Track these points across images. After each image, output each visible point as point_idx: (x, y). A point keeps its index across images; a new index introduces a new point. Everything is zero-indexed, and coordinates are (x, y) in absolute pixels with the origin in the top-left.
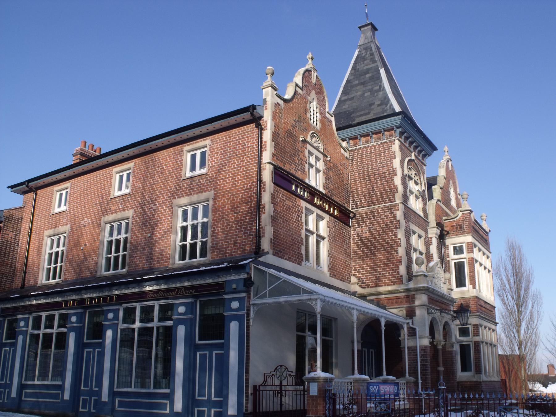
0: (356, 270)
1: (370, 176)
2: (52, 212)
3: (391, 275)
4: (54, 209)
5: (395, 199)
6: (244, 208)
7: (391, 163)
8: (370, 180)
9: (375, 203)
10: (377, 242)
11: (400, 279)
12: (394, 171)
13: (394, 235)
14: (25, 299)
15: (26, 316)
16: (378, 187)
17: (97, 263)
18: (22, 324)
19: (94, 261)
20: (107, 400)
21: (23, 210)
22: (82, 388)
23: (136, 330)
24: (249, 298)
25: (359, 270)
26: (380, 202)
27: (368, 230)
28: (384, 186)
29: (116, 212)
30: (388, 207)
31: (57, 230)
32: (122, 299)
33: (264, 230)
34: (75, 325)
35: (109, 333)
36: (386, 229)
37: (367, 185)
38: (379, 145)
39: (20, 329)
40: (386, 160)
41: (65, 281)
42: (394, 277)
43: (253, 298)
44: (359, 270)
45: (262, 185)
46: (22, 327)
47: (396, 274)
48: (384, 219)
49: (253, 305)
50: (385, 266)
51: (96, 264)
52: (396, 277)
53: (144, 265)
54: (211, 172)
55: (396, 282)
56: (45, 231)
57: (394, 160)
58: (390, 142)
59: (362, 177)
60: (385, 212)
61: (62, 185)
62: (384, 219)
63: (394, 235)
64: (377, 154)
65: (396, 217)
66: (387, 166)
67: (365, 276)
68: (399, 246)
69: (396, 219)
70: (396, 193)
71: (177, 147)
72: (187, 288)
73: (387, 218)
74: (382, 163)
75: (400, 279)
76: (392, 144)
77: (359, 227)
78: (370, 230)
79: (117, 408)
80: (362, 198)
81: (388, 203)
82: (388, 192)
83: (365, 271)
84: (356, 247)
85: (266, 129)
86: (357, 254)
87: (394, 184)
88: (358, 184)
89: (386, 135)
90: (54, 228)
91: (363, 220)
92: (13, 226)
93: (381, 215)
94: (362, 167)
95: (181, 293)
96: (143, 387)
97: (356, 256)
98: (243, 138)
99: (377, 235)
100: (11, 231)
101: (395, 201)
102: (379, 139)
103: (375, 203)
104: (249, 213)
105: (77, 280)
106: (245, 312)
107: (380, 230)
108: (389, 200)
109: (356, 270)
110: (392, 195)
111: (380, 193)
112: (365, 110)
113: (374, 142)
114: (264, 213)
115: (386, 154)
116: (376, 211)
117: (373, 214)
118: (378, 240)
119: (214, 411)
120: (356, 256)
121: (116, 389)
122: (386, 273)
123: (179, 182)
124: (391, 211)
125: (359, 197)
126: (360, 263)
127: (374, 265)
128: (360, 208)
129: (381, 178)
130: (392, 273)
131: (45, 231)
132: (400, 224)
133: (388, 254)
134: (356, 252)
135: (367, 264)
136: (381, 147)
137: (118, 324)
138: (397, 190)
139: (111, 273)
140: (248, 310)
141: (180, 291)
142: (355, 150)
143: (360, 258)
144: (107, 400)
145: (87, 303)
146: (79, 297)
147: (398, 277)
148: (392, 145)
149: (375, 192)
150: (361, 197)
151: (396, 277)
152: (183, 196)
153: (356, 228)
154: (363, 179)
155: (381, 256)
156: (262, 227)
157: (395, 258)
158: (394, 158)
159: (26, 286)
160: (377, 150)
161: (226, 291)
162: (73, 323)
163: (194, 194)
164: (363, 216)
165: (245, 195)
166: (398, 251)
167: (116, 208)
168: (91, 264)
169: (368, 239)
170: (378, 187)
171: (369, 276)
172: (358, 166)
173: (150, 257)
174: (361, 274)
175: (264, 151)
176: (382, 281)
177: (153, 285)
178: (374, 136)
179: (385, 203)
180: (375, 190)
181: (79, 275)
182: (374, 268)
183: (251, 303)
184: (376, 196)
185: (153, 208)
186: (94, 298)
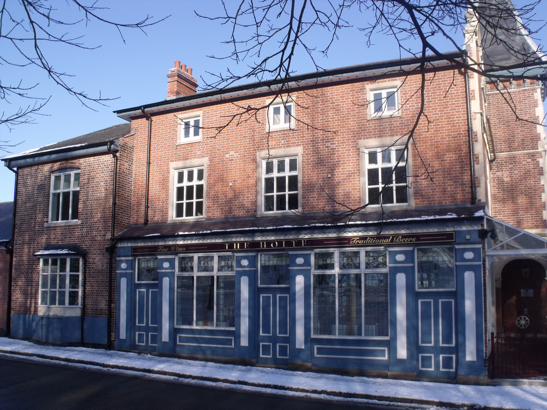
0: (497, 212)
1: (510, 122)
2: (178, 143)
3: (534, 219)
4: (180, 140)
5: (537, 147)
6: (450, 157)
7: (533, 111)
8: (510, 126)
9: (516, 148)
10: (519, 187)
11: (544, 223)
12: (537, 119)
13: (537, 181)
14: (166, 239)
15: (173, 257)
16: (519, 133)
17: (256, 201)
18: (166, 265)
19: (251, 199)
20: (303, 347)
21: (134, 138)
22: (261, 334)
23: (337, 275)
24: (484, 249)
25: (500, 212)
26: (522, 148)
27: (509, 175)
28: (525, 133)
29: (277, 148)
30: (531, 154)
31: (188, 163)
32: (312, 244)
33: (479, 180)
34: (247, 269)
35: (300, 280)
36: (527, 175)
37: (507, 130)
38: (519, 92)
39: (163, 271)
40: (527, 107)
41: (209, 219)
42: (537, 221)
43: (488, 249)
44: (500, 212)
45: (473, 134)
46: (166, 269)
47: (540, 219)
48: (526, 165)
49: (488, 255)
50: (527, 210)
51: (255, 203)
52: (539, 221)
53: (325, 207)
54: (406, 115)
55: (539, 225)
56: (170, 163)
57: (536, 109)
58: (531, 90)
59: (501, 123)
60: (527, 158)
61: (189, 112)
62: (526, 165)
63: (537, 181)
64: (517, 100)
65: (539, 164)
66: (529, 114)
67: (507, 218)
68: (542, 192)
69: (539, 166)
70: (539, 140)
71: (356, 84)
72: (404, 236)
73: (529, 165)
74: (523, 110)
75: (544, 223)
76: (533, 92)
77: (500, 171)
78: (511, 175)
79: (316, 355)
80: (502, 143)
81: (530, 150)
82: (530, 139)
83: (507, 214)
84: (496, 190)
85: (473, 78)
86: (497, 197)
87: (536, 132)
88: (497, 129)
89: (528, 82)
90: (183, 160)
91: (504, 164)
92: (127, 155)
93: (523, 161)
94: (501, 112)
95: (397, 240)
96: (350, 333)
97: (497, 199)
98: (444, 84)
99: (519, 180)
100: (126, 162)
101: (538, 149)
102: (518, 85)
103: (516, 148)
104: (459, 162)
105: (226, 218)
106: (481, 263)
107: (522, 176)
108: (531, 147)
109: (497, 212)
110: (534, 143)
111: (521, 140)
112: (503, 54)
113: (514, 88)
114: (478, 164)
115: (528, 101)
116: (517, 157)
117: (513, 160)
118: (519, 185)
119: (443, 357)
120: (497, 199)
121: (313, 336)
122: (529, 217)
123: (364, 122)
124: (533, 158)
125: (498, 142)
126: (501, 205)
127: (516, 209)
128: (499, 152)
129: (522, 125)
130: (535, 217)
131: (170, 163)
132: (544, 171)
133: (531, 199)
134: (496, 195)
135: (509, 207)
136: (521, 94)
137: (310, 270)
138: (539, 138)
139: (274, 214)
140: (484, 261)
141: (396, 239)
142: (493, 94)
143: (501, 201)
144: (303, 347)
145: (263, 246)
146: (250, 239)
147: (541, 221)
148: (535, 93)
149: (516, 138)
150: (501, 141)
151: (539, 221)
152: (372, 137)
153: (496, 171)
154: (502, 125)
155: (522, 200)
156: (477, 178)
157: (538, 203)
158: (537, 107)
159: (149, 222)
160: (517, 96)
161: (457, 241)
162: (244, 267)
163: (386, 136)
164: (503, 160)
165: (452, 143)
166: (541, 196)
167: (277, 143)
168: (247, 202)
169: (509, 183)
170: (519, 133)
171: (511, 218)
172: (497, 111)
173: (332, 199)
174: (503, 216)
175: (472, 99)
176: (525, 224)
177: (360, 231)
178: (514, 82)
179: (527, 150)
180: (515, 136)
181: (229, 213)
182: (515, 212)
183: (487, 254)
184: (517, 142)
185: (330, 147)
186: (274, 242)
